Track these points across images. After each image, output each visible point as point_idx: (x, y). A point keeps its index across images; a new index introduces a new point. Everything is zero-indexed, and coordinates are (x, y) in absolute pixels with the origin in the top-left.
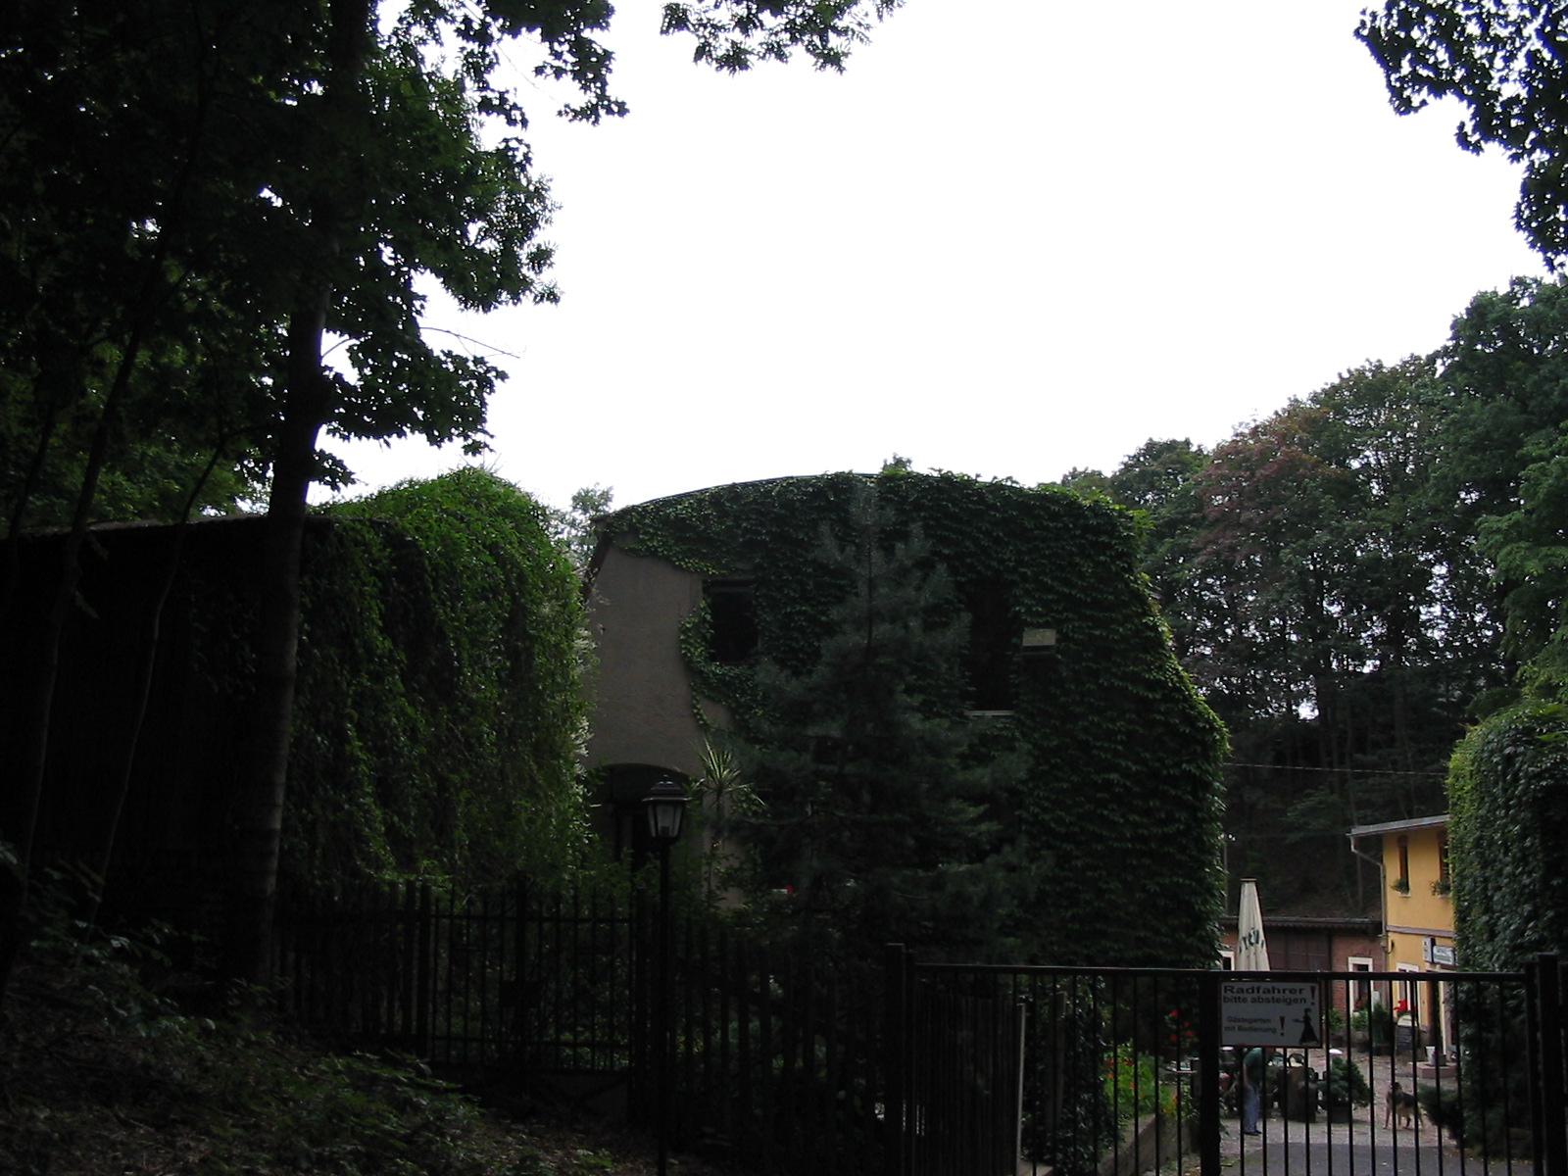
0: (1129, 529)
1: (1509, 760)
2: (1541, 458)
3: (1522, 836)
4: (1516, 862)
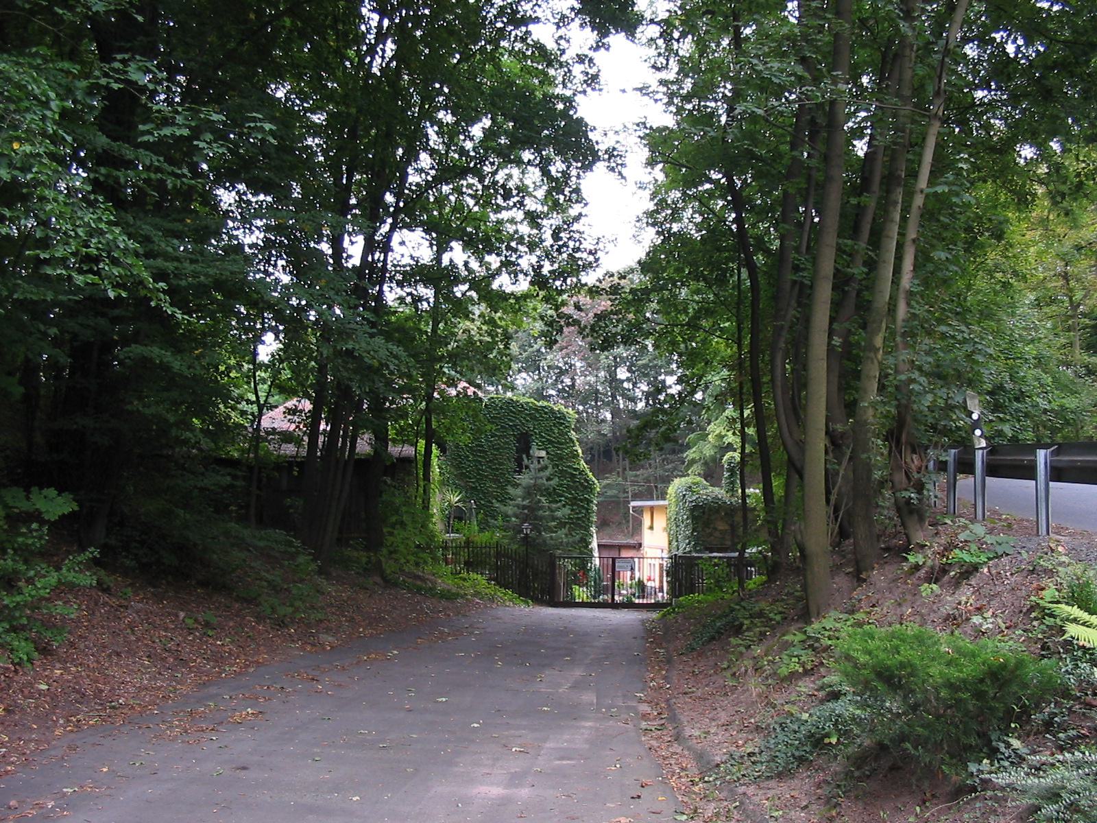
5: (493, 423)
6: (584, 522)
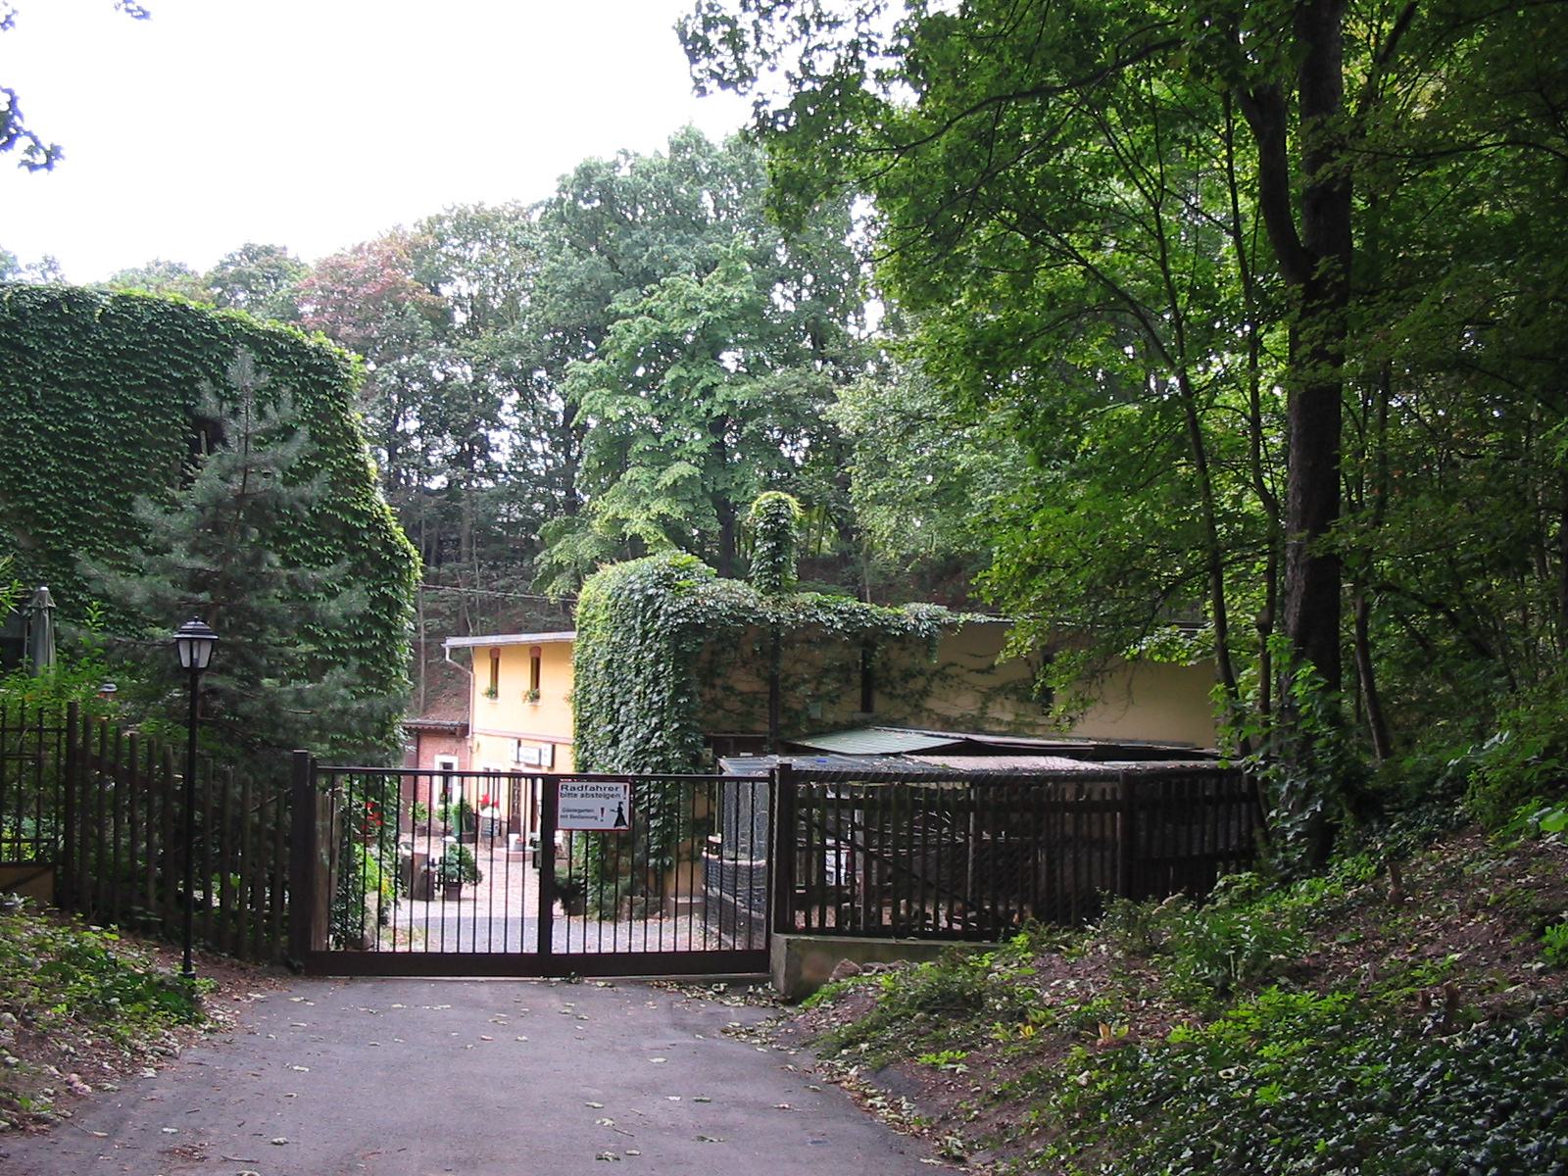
0: (348, 372)
1: (650, 599)
2: (625, 316)
3: (656, 662)
4: (647, 683)
5: (126, 368)
6: (376, 662)
